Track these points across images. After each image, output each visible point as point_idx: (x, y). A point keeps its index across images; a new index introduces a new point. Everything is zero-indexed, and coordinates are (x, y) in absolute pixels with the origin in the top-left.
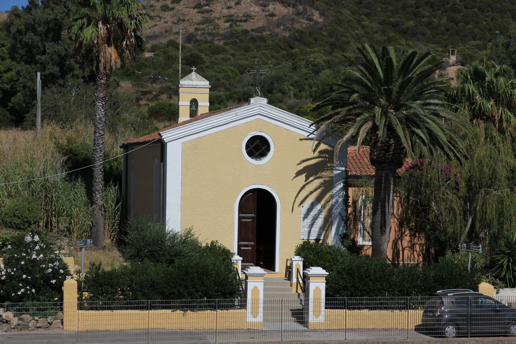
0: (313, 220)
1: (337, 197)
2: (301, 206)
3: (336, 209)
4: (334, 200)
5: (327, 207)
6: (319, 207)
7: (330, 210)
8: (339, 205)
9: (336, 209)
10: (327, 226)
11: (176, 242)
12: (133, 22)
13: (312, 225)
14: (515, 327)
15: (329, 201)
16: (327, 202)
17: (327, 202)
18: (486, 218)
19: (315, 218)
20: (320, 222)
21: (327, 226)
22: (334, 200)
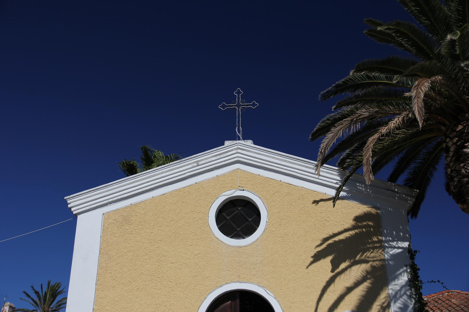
1: (405, 297)
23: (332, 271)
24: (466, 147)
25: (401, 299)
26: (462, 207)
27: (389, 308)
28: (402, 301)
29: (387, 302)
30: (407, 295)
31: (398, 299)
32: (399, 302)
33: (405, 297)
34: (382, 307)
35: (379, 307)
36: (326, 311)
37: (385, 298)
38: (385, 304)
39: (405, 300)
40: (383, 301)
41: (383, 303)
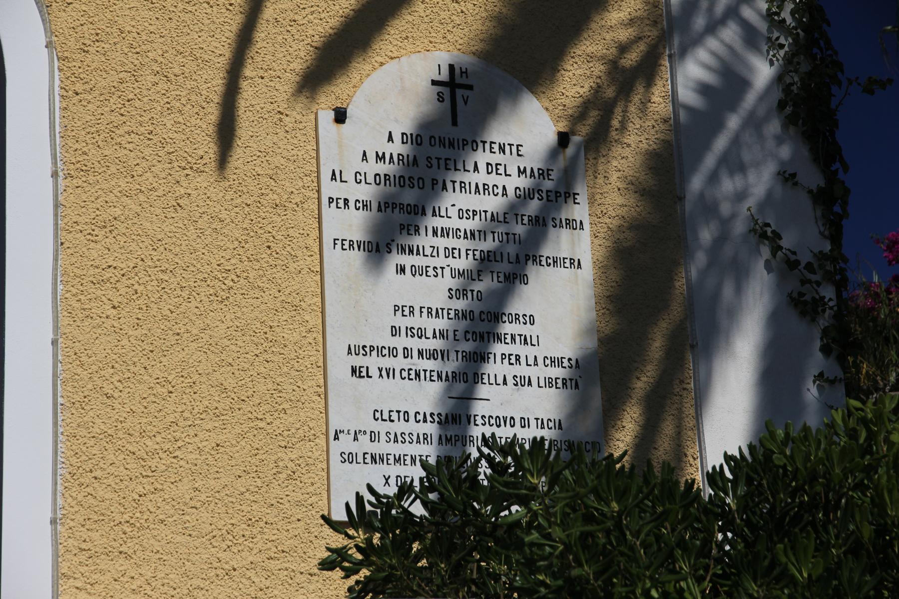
0: (486, 260)
1: (730, 33)
2: (322, 522)
3: (732, 162)
4: (693, 71)
5: (626, 157)
6: (529, 129)
7: (665, 171)
8: (753, 123)
9: (732, 162)
10: (657, 346)
11: (523, 561)
12: (72, 274)
13: (478, 329)
14: (343, 592)
15: (647, 71)
16: (628, 77)
17: (628, 77)
18: (797, 470)
19: (509, 257)
20: (559, 307)
21: (657, 346)
22: (693, 71)
23: (421, 595)
24: (668, 4)
25: (712, 43)
26: (677, 58)
27: (650, 83)
28: (714, 54)
29: (642, 47)
30: (746, 25)
31: (697, 41)
32: (702, 54)
33: (730, 33)
34: (614, 67)
35: (599, 69)
36: (268, 4)
37: (631, 22)
38: (632, 58)
39: (730, 47)
40: (624, 35)
41: (623, 48)
